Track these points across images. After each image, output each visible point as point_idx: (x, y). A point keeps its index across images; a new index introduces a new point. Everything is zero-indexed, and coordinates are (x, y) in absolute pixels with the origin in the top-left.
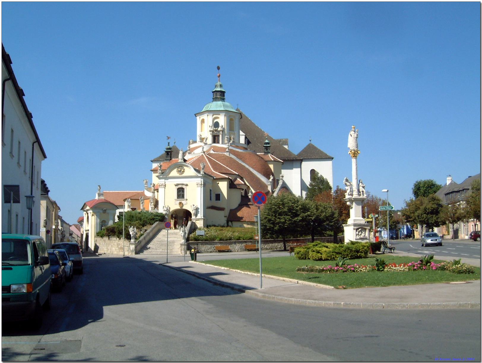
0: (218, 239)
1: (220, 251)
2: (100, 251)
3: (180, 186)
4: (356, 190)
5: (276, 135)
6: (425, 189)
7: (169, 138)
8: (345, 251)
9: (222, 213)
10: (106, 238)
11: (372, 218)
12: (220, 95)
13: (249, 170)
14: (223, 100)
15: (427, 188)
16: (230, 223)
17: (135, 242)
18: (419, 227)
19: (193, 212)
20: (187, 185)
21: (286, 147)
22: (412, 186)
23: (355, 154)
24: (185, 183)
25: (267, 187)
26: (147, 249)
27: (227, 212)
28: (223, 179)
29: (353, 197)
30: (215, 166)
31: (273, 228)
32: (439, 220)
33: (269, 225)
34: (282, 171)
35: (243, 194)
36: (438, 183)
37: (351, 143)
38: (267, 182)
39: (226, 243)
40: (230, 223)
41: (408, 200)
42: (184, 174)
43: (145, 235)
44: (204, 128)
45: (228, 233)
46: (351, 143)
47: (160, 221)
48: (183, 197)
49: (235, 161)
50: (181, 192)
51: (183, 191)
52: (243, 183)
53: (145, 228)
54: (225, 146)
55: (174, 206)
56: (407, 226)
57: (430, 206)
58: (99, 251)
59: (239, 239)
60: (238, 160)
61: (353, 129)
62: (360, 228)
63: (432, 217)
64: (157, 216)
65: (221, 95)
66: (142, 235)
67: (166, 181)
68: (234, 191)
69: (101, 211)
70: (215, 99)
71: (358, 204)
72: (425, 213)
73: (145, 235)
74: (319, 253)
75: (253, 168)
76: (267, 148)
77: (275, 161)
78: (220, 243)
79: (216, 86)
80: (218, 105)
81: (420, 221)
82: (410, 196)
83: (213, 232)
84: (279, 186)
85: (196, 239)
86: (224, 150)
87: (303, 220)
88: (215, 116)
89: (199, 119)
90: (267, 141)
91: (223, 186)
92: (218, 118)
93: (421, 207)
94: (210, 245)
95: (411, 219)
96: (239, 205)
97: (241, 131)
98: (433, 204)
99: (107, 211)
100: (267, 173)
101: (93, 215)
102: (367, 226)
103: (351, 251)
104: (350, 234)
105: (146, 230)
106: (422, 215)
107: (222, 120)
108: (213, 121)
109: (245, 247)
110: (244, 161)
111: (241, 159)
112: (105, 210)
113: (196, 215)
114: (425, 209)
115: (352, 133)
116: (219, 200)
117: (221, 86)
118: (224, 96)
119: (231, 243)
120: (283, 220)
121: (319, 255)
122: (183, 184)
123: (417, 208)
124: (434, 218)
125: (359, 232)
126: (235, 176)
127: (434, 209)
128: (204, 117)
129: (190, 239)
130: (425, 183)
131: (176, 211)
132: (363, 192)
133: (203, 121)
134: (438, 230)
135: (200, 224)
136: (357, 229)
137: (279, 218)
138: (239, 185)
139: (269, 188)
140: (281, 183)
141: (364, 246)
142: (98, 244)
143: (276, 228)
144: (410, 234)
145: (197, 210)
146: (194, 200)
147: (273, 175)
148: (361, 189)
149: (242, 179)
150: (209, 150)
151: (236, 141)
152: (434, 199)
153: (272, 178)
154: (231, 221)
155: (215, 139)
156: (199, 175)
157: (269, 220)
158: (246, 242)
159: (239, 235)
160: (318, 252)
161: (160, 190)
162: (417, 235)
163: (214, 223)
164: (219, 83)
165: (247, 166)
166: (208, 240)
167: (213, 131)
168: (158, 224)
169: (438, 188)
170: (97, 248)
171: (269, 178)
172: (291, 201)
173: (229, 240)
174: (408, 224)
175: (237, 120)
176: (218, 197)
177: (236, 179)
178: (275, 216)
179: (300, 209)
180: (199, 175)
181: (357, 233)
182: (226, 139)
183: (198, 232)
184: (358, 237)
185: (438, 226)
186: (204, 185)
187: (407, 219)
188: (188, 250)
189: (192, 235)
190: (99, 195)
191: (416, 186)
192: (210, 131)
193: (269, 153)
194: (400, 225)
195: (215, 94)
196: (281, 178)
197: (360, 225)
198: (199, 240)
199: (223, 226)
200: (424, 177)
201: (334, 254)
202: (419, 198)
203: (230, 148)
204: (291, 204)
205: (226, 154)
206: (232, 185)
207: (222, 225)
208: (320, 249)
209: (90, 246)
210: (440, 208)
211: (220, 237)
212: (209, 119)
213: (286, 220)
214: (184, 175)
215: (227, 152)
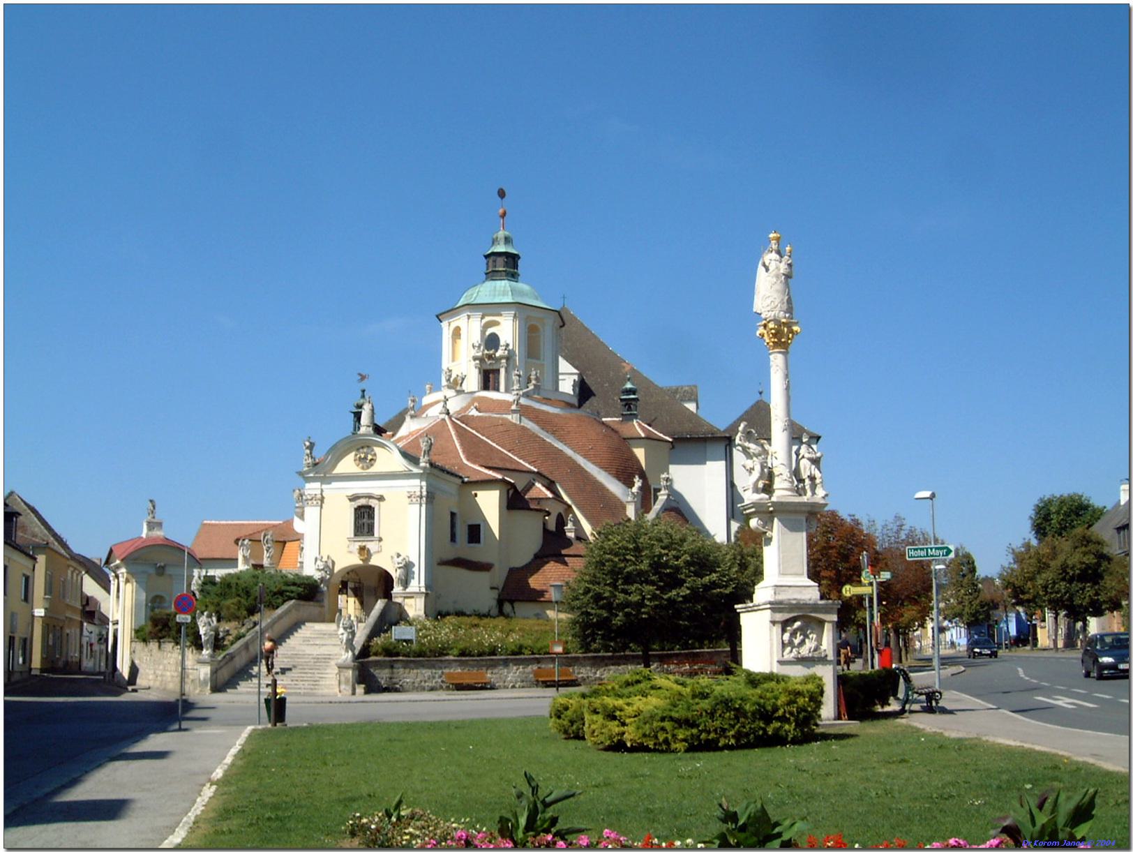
0: (456, 652)
1: (460, 687)
2: (140, 681)
3: (362, 502)
4: (786, 473)
5: (663, 379)
6: (1062, 518)
7: (363, 378)
8: (712, 714)
9: (482, 578)
10: (153, 645)
11: (871, 584)
12: (507, 265)
13: (574, 462)
14: (513, 276)
15: (1067, 515)
16: (507, 608)
17: (212, 656)
18: (1049, 616)
19: (395, 575)
20: (381, 499)
21: (691, 406)
22: (1030, 511)
23: (782, 337)
24: (377, 492)
25: (624, 508)
26: (251, 676)
27: (498, 576)
28: (487, 484)
29: (774, 499)
30: (474, 449)
31: (608, 620)
32: (1101, 598)
33: (597, 613)
34: (672, 468)
35: (552, 526)
36: (1097, 501)
37: (767, 295)
38: (625, 495)
39: (479, 665)
40: (507, 608)
41: (1018, 544)
42: (377, 468)
43: (248, 637)
44: (460, 350)
45: (490, 634)
46: (767, 295)
47: (301, 597)
48: (370, 531)
49: (535, 437)
50: (364, 519)
51: (371, 517)
52: (550, 495)
53: (256, 618)
54: (510, 397)
55: (346, 558)
56: (1018, 614)
57: (1077, 559)
58: (139, 681)
59: (519, 650)
60: (543, 435)
61: (774, 245)
62: (796, 619)
63: (1083, 589)
64: (294, 584)
65: (506, 264)
66: (239, 638)
67: (324, 486)
68: (519, 516)
69: (152, 571)
70: (491, 275)
71: (792, 527)
72: (1063, 579)
73: (248, 637)
74: (614, 718)
75: (585, 456)
76: (628, 404)
77: (649, 438)
78: (462, 664)
79: (494, 242)
80: (499, 290)
81: (1050, 601)
82: (1022, 533)
83: (445, 632)
84: (657, 507)
85: (389, 651)
86: (503, 406)
87: (695, 596)
88: (487, 319)
89: (447, 328)
90: (629, 386)
91: (489, 503)
92: (496, 323)
93: (1052, 563)
94: (433, 667)
95: (1026, 597)
96: (536, 556)
97: (561, 359)
98: (1085, 554)
99: (169, 571)
100: (626, 471)
101: (127, 581)
102: (826, 610)
103: (740, 713)
104: (760, 645)
105: (255, 624)
106: (1054, 583)
107: (507, 330)
108: (483, 332)
109: (536, 674)
110: (561, 439)
111: (553, 433)
112: (163, 568)
113: (405, 583)
114: (1064, 568)
115: (770, 258)
116: (478, 541)
117: (507, 240)
118: (516, 266)
119: (493, 665)
120: (635, 598)
121: (614, 727)
122: (370, 497)
123: (1043, 566)
124: (1089, 591)
125: (793, 634)
126: (527, 478)
127: (1088, 567)
128: (460, 321)
129: (373, 650)
130: (1062, 502)
131: (352, 571)
132: (812, 478)
133: (457, 333)
134: (1099, 624)
135: (415, 608)
136: (785, 624)
137: (625, 592)
138: (539, 500)
139: (631, 512)
140: (663, 496)
141: (798, 694)
142: (137, 662)
143: (619, 620)
144: (1026, 636)
145: (407, 567)
146: (403, 539)
147: (643, 476)
148: (806, 468)
149: (550, 486)
150: (467, 408)
151: (548, 385)
152: (1086, 541)
153: (638, 483)
154: (512, 602)
155: (488, 379)
156: (416, 470)
157: (598, 598)
158: (538, 661)
159: (522, 642)
160: (611, 716)
161: (308, 510)
162: (1044, 637)
163: (459, 607)
164: (501, 234)
165: (569, 452)
166: (426, 655)
167: (481, 360)
168: (293, 606)
169: (1097, 514)
170: (134, 670)
171: (630, 484)
172: (660, 540)
173: (490, 656)
174: (1021, 609)
175: (550, 330)
176: (475, 532)
177: (530, 486)
178: (615, 587)
179: (688, 564)
180: (416, 470)
181: (786, 636)
182: (515, 378)
183: (400, 632)
184: (789, 655)
185: (1098, 613)
186: (431, 498)
187: (1016, 597)
188: (359, 683)
189: (378, 641)
190: (151, 525)
191: (1039, 510)
192: (475, 359)
193: (635, 416)
194: (998, 614)
195: (491, 260)
196: (663, 483)
197: (798, 606)
198: (397, 654)
199: (481, 616)
200: (1060, 487)
201: (667, 725)
202: (1048, 539)
203: (523, 401)
204: (657, 550)
205: (509, 417)
206: (515, 501)
207: (485, 610)
208: (620, 702)
209: (118, 666)
210: (1105, 564)
211: (462, 645)
212: (471, 328)
213: (644, 598)
214: (373, 470)
215: (514, 412)
